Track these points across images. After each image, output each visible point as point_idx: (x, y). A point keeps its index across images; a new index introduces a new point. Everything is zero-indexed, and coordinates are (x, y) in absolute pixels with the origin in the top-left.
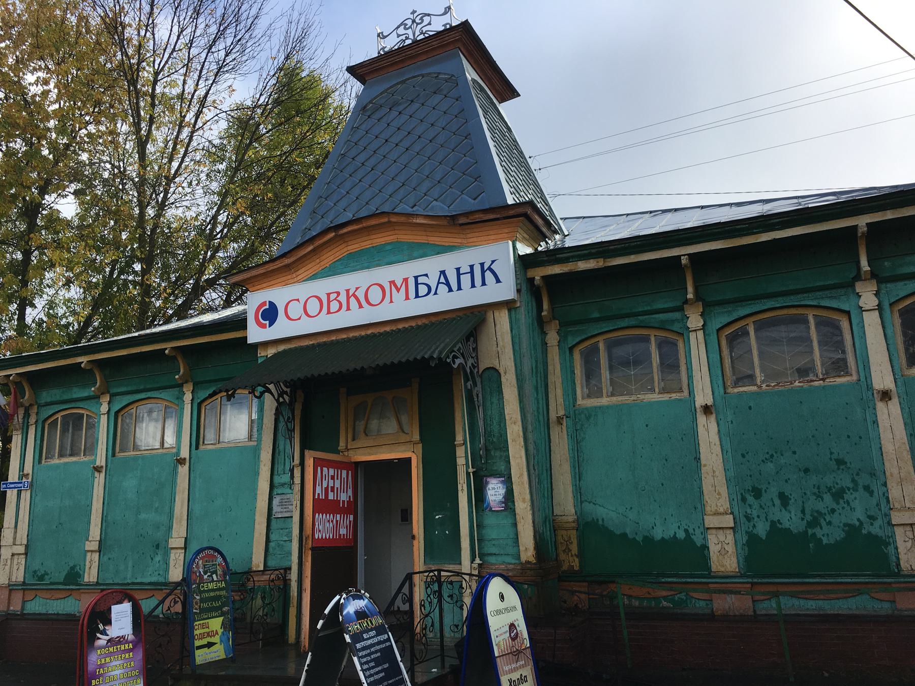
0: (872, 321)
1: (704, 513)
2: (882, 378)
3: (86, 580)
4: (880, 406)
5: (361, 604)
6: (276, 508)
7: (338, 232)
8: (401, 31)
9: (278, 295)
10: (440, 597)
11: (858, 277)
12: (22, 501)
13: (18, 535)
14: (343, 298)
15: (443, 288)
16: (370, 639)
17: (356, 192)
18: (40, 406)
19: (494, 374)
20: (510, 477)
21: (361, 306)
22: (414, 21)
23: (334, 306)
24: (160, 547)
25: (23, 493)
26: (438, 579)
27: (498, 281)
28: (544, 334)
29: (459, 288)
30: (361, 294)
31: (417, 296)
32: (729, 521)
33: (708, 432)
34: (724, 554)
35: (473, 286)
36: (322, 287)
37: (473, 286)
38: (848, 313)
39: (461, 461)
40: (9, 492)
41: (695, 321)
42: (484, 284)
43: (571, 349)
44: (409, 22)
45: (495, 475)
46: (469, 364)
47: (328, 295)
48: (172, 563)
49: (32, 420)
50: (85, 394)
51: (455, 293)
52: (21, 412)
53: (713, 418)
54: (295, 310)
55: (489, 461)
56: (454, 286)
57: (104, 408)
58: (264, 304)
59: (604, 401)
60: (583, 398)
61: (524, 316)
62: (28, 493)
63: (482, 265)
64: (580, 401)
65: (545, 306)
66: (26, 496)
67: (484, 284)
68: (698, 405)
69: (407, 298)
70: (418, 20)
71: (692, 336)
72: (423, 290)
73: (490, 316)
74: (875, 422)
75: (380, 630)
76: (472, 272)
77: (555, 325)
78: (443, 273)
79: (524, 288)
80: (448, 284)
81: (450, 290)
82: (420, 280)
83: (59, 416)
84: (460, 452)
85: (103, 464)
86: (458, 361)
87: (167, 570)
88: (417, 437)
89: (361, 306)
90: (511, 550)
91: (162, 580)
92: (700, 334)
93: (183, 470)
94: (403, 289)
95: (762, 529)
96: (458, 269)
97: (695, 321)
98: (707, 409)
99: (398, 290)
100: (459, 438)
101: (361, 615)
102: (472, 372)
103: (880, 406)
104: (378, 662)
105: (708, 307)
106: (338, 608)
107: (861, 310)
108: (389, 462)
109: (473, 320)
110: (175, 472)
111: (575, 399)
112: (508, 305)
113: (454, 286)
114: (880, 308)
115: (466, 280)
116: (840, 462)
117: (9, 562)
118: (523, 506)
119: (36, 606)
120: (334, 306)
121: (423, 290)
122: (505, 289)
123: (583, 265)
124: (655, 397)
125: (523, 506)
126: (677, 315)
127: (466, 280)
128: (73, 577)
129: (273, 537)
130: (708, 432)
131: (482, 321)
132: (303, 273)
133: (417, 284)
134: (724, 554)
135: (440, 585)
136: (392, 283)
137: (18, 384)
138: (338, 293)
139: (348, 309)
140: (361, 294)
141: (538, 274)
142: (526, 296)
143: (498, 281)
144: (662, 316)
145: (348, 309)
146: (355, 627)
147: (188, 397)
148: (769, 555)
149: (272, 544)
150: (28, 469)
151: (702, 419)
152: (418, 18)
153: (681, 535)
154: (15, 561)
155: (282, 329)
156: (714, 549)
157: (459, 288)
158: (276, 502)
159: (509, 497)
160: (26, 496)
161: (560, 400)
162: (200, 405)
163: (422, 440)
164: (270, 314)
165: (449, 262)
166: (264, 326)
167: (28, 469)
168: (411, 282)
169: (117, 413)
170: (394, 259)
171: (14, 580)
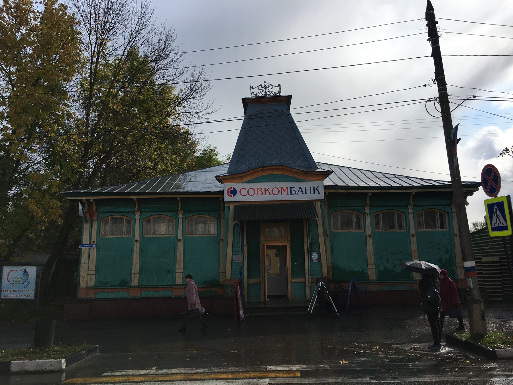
0: (411, 216)
1: (131, 269)
2: (412, 231)
3: (132, 284)
4: (412, 238)
6: (234, 259)
7: (263, 168)
8: (260, 87)
9: (238, 186)
11: (409, 204)
12: (91, 254)
14: (263, 190)
15: (300, 193)
20: (320, 252)
21: (270, 194)
22: (265, 86)
23: (260, 193)
24: (171, 271)
25: (91, 250)
27: (319, 193)
29: (306, 193)
30: (270, 190)
31: (291, 194)
32: (374, 266)
33: (370, 242)
34: (372, 274)
35: (311, 193)
37: (311, 193)
38: (405, 213)
39: (306, 247)
40: (83, 249)
41: (367, 211)
42: (314, 193)
44: (264, 86)
45: (315, 252)
47: (258, 189)
51: (304, 195)
54: (244, 192)
55: (314, 246)
56: (304, 193)
58: (231, 188)
59: (340, 231)
63: (314, 187)
66: (94, 251)
67: (314, 193)
68: (367, 234)
69: (288, 194)
70: (267, 86)
71: (366, 214)
72: (293, 192)
74: (410, 242)
76: (310, 189)
78: (300, 188)
80: (302, 191)
81: (303, 194)
82: (292, 189)
84: (306, 244)
88: (289, 239)
89: (270, 194)
91: (172, 284)
94: (286, 191)
95: (382, 269)
96: (306, 188)
97: (367, 211)
98: (370, 236)
103: (412, 238)
105: (371, 207)
109: (310, 204)
112: (320, 201)
113: (304, 193)
115: (308, 191)
116: (401, 252)
117: (86, 278)
119: (102, 295)
120: (260, 193)
121: (293, 192)
122: (320, 196)
123: (341, 191)
125: (323, 261)
126: (362, 208)
127: (308, 191)
128: (125, 284)
130: (370, 242)
132: (245, 179)
133: (291, 190)
134: (372, 274)
136: (282, 188)
138: (261, 189)
139: (265, 194)
140: (270, 190)
143: (319, 193)
145: (265, 194)
148: (384, 275)
151: (368, 238)
152: (266, 85)
153: (361, 270)
154: (89, 277)
155: (238, 198)
156: (370, 273)
157: (306, 193)
158: (234, 257)
159: (319, 258)
164: (233, 192)
165: (304, 185)
166: (231, 196)
171: (89, 285)
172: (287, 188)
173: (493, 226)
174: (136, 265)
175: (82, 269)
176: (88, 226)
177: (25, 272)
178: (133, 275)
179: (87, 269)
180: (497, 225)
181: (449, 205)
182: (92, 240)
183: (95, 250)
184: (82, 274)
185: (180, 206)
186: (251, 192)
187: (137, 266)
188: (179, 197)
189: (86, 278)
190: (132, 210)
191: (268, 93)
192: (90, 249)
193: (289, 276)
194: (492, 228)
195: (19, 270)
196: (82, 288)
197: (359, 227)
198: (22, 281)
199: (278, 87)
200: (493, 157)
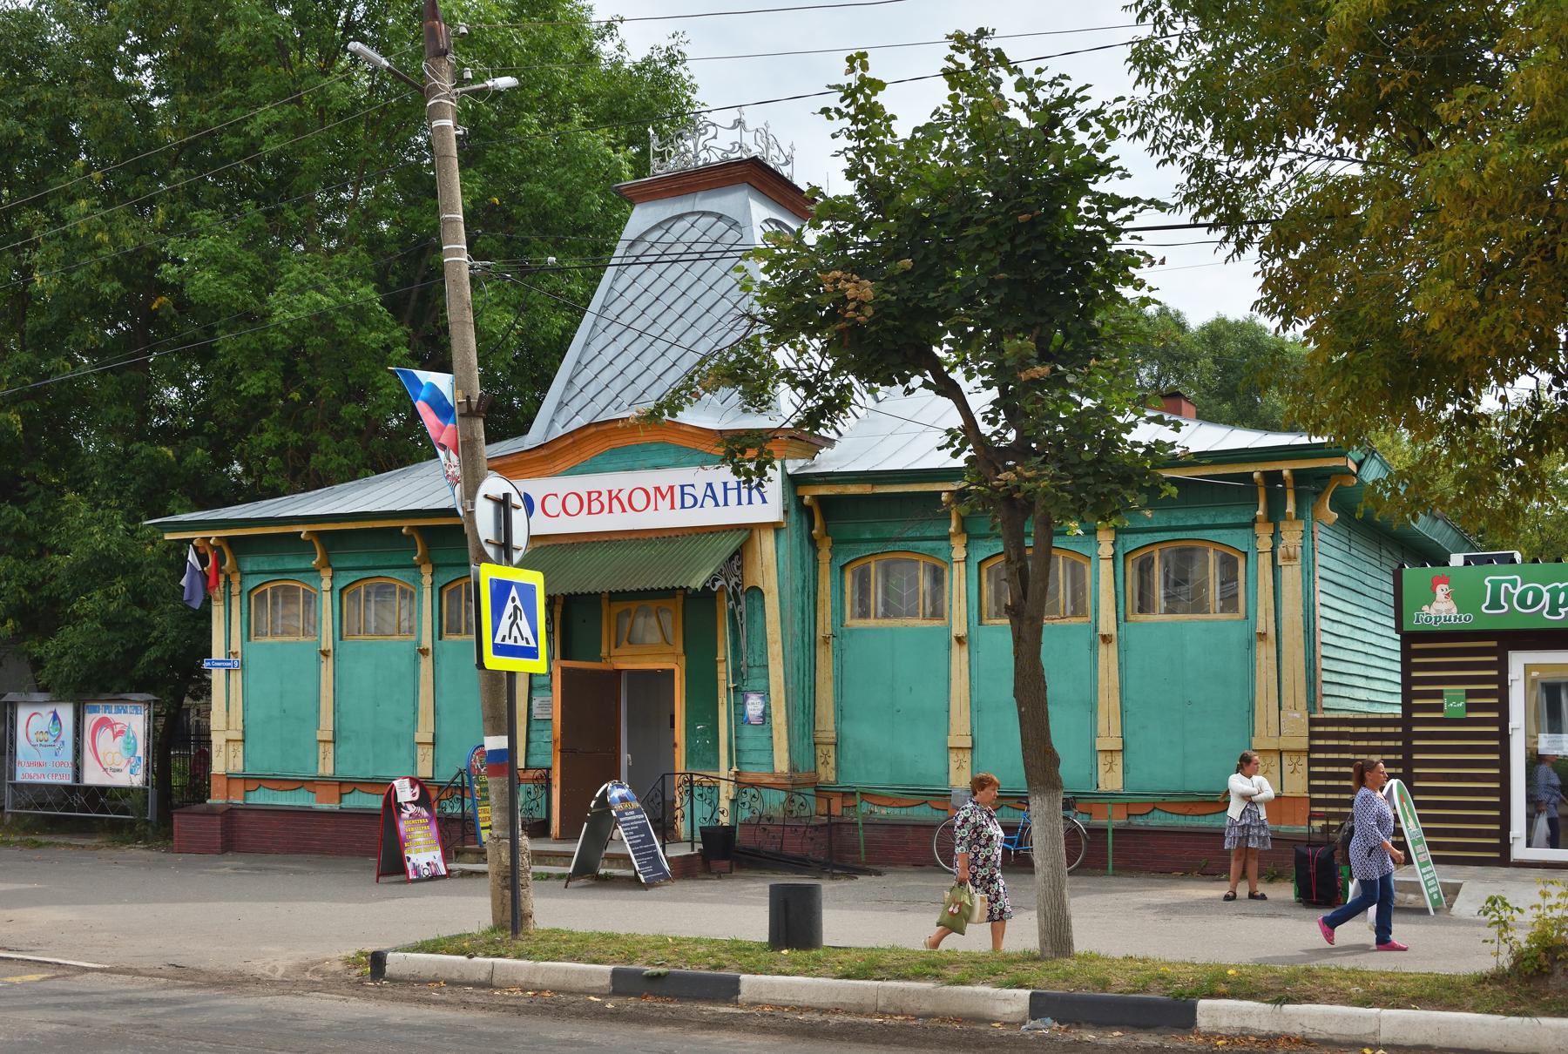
5: (624, 792)
6: (535, 710)
10: (692, 796)
13: (232, 719)
14: (605, 499)
15: (709, 502)
16: (630, 816)
17: (620, 363)
18: (244, 574)
19: (757, 593)
23: (596, 506)
26: (691, 781)
27: (764, 501)
28: (816, 550)
29: (726, 504)
30: (624, 497)
31: (683, 507)
35: (740, 503)
36: (583, 483)
37: (740, 503)
39: (722, 676)
40: (214, 671)
42: (750, 502)
43: (843, 568)
46: (732, 583)
47: (589, 494)
48: (420, 758)
49: (235, 589)
50: (303, 565)
51: (722, 508)
52: (222, 579)
53: (965, 648)
54: (553, 506)
56: (721, 501)
57: (326, 584)
60: (852, 617)
61: (791, 538)
62: (239, 675)
64: (848, 621)
65: (817, 524)
66: (236, 678)
67: (750, 502)
69: (673, 507)
71: (955, 566)
72: (689, 501)
73: (756, 533)
75: (637, 812)
77: (828, 542)
78: (710, 485)
79: (793, 507)
80: (714, 497)
81: (717, 505)
82: (687, 490)
83: (268, 587)
84: (721, 668)
85: (330, 647)
86: (718, 584)
87: (415, 765)
88: (680, 649)
90: (765, 759)
92: (963, 565)
93: (426, 664)
96: (725, 484)
98: (959, 640)
99: (663, 497)
100: (720, 657)
101: (623, 799)
102: (735, 592)
104: (636, 832)
105: (972, 538)
106: (605, 793)
107: (1099, 558)
108: (654, 671)
110: (416, 662)
111: (843, 620)
112: (776, 527)
113: (721, 501)
114: (1114, 557)
118: (779, 718)
121: (689, 501)
123: (853, 489)
124: (918, 622)
126: (944, 544)
127: (733, 495)
129: (533, 736)
131: (750, 539)
132: (561, 465)
135: (692, 786)
136: (657, 489)
137: (218, 550)
138: (600, 494)
140: (624, 497)
141: (808, 494)
142: (793, 517)
143: (764, 501)
144: (929, 544)
146: (619, 807)
147: (427, 580)
149: (532, 745)
150: (236, 646)
157: (726, 504)
158: (535, 703)
159: (766, 715)
160: (236, 678)
161: (828, 620)
162: (441, 589)
163: (685, 653)
167: (236, 646)
168: (677, 491)
169: (342, 591)
170: (658, 461)
172: (671, 488)
173: (498, 640)
177: (55, 717)
180: (509, 642)
185: (1262, 505)
186: (573, 504)
188: (405, 525)
190: (1246, 519)
191: (703, 155)
194: (495, 645)
195: (46, 712)
197: (937, 613)
198: (51, 742)
199: (734, 128)
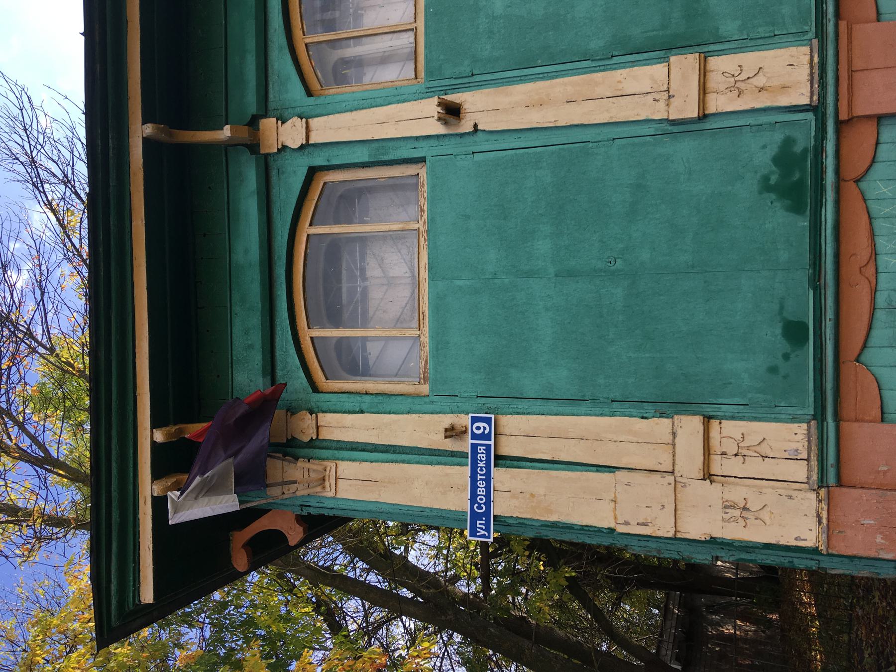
25: (509, 448)
66: (520, 432)
117: (737, 493)
171: (799, 471)
174: (645, 91)
175: (662, 526)
176: (347, 468)
178: (717, 103)
179: (660, 487)
181: (267, 165)
182: (437, 440)
183: (510, 423)
184: (700, 524)
187: (645, 77)
189: (737, 493)
192: (501, 460)
193: (521, 91)
196: (830, 527)
200: (229, 540)
